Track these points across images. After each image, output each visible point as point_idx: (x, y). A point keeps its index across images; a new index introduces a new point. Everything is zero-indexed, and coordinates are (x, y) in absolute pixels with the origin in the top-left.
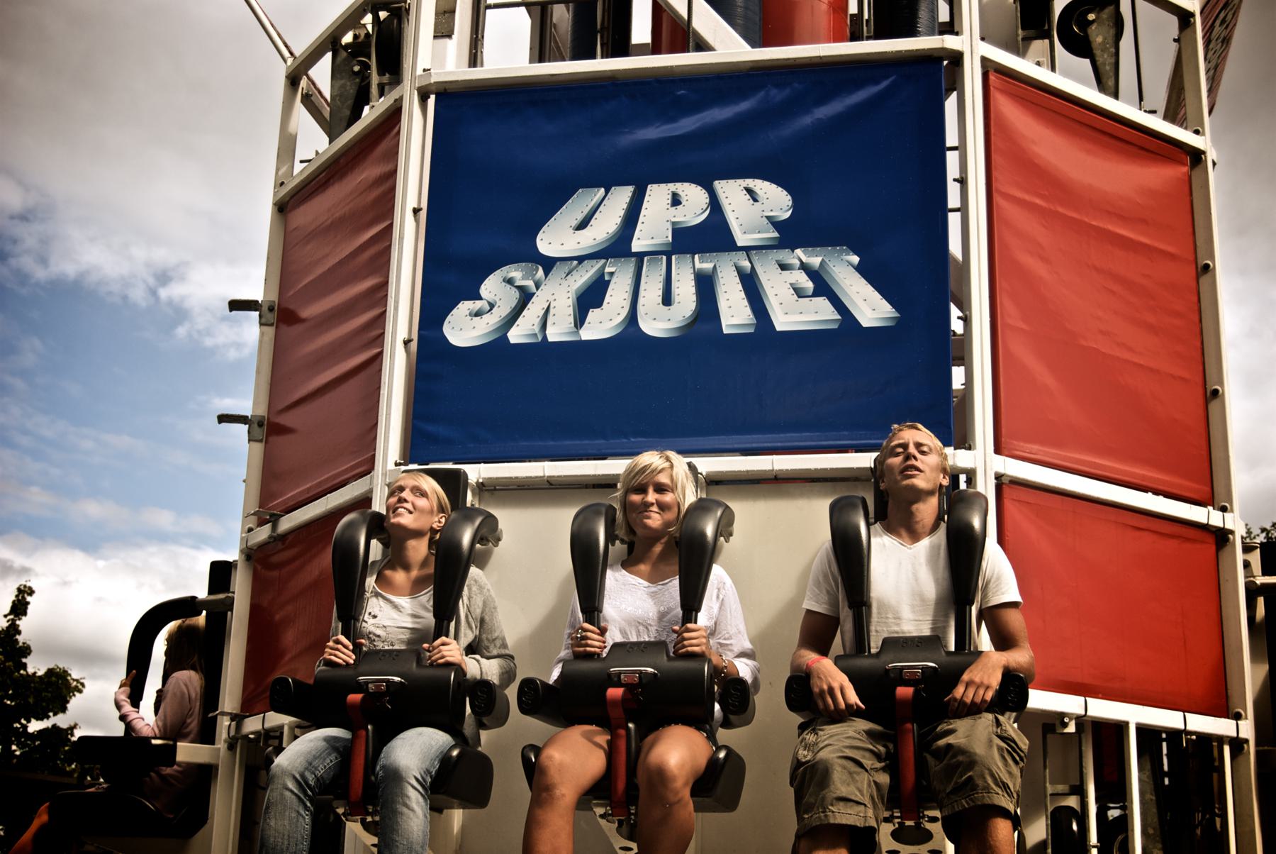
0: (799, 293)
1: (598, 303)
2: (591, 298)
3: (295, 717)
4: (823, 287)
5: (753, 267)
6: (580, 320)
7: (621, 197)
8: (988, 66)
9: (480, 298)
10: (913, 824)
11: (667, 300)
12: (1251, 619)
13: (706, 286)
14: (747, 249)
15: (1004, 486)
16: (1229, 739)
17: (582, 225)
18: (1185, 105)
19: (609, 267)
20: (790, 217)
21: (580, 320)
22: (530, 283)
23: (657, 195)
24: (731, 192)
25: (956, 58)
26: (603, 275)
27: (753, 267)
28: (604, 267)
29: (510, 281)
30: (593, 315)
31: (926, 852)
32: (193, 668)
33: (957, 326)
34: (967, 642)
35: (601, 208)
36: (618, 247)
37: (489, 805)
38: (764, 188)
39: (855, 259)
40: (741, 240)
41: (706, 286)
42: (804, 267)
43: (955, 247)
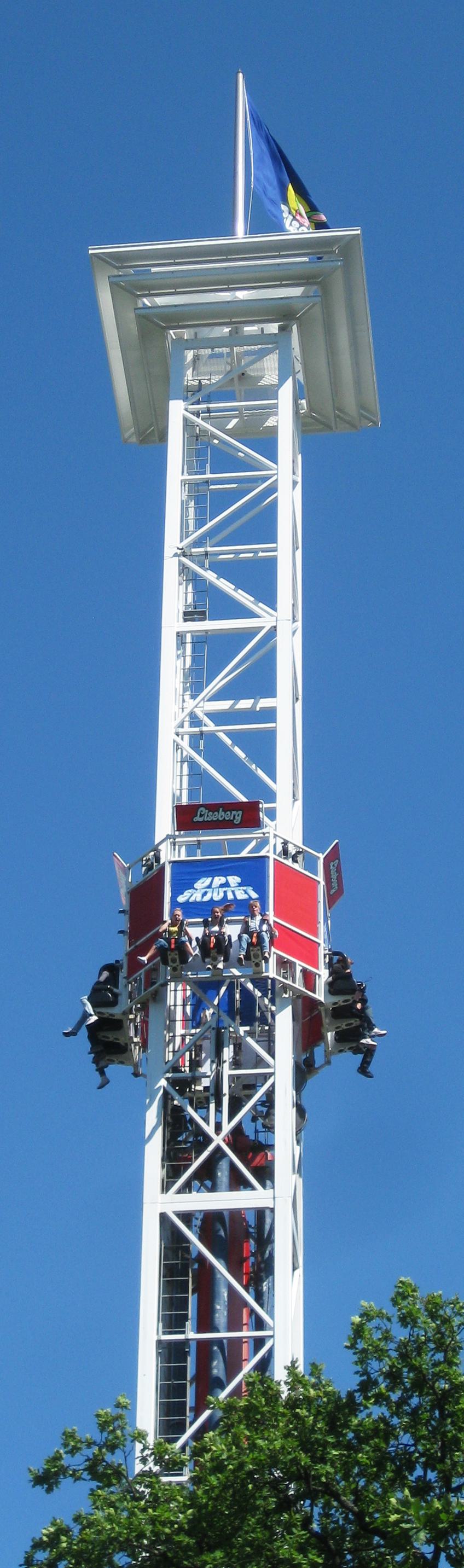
1: (206, 895)
2: (205, 894)
7: (210, 879)
13: (225, 892)
15: (190, 1342)
18: (141, 1470)
19: (314, 992)
20: (238, 876)
23: (216, 879)
30: (205, 897)
31: (353, 1375)
33: (242, 455)
36: (209, 886)
37: (87, 1040)
38: (236, 877)
39: (252, 888)
40: (231, 886)
41: (225, 892)
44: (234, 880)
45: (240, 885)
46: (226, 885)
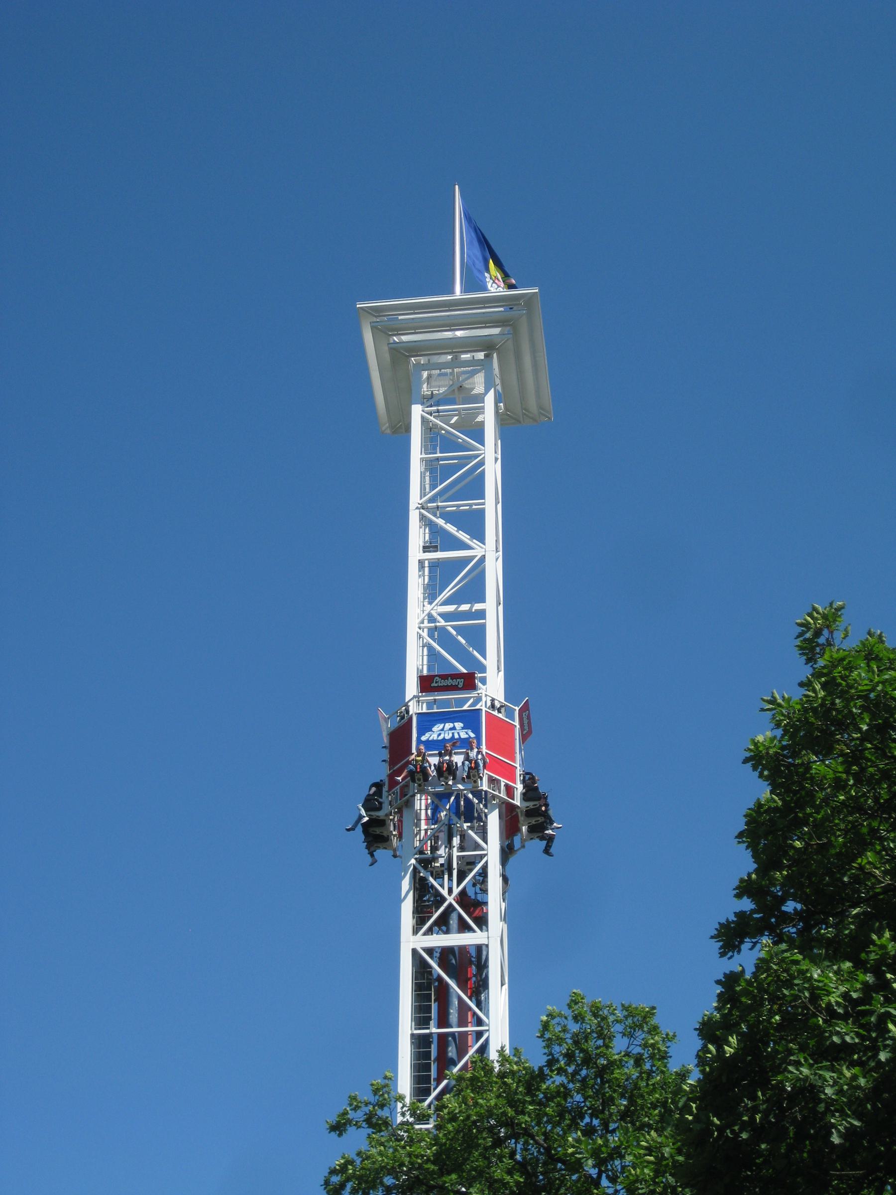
3: (364, 823)
4: (467, 733)
6: (438, 737)
7: (443, 725)
8: (486, 711)
12: (520, 779)
21: (438, 737)
23: (447, 724)
25: (482, 710)
32: (463, 723)
34: (463, 483)
36: (442, 730)
38: (460, 723)
43: (474, 541)
44: (459, 725)
45: (463, 728)
46: (454, 728)
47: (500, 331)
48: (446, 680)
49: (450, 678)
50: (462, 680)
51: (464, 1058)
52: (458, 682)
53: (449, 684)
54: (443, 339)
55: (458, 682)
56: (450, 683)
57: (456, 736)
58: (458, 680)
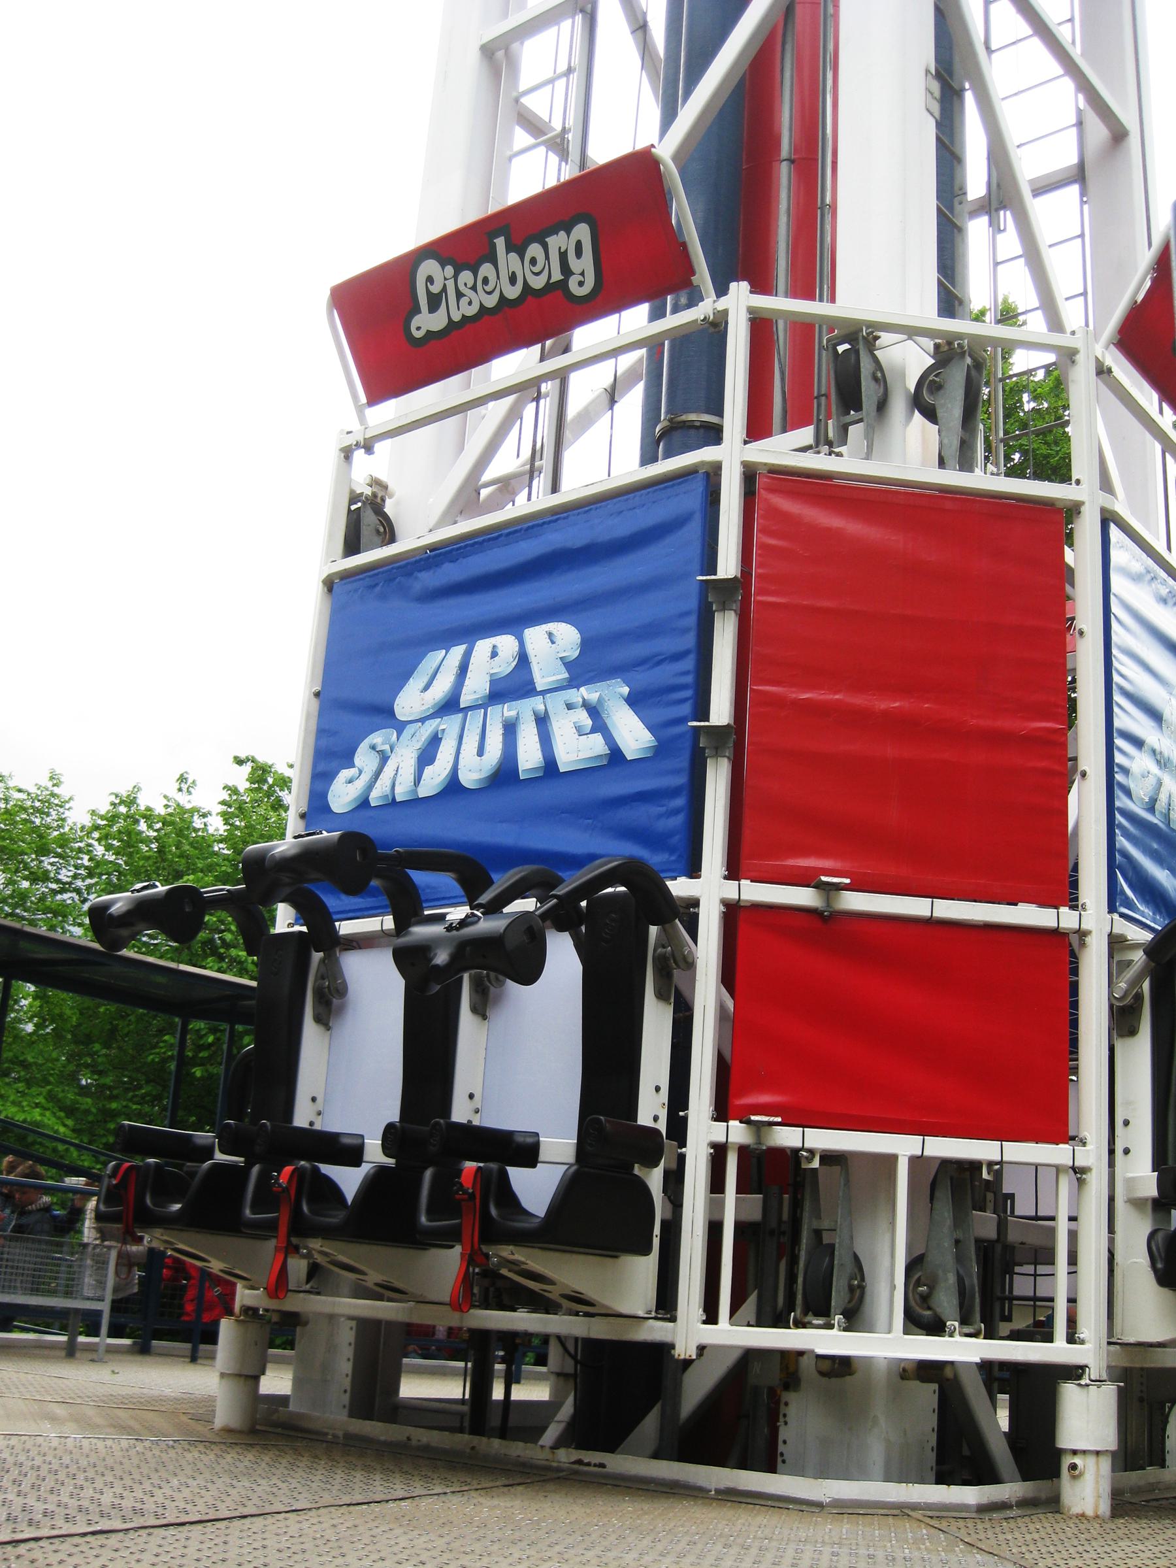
0: (580, 731)
2: (427, 757)
5: (546, 709)
9: (353, 766)
10: (644, 1119)
11: (480, 753)
13: (510, 729)
14: (543, 693)
16: (939, 1161)
17: (426, 688)
22: (387, 747)
23: (483, 647)
24: (535, 636)
26: (437, 734)
27: (546, 709)
28: (439, 725)
29: (373, 747)
30: (428, 771)
35: (440, 670)
42: (586, 705)
47: (554, 153)
48: (486, 269)
49: (500, 242)
50: (582, 232)
51: (871, 476)
52: (563, 256)
53: (513, 292)
54: (434, 414)
55: (563, 256)
56: (513, 279)
57: (529, 757)
58: (557, 241)
